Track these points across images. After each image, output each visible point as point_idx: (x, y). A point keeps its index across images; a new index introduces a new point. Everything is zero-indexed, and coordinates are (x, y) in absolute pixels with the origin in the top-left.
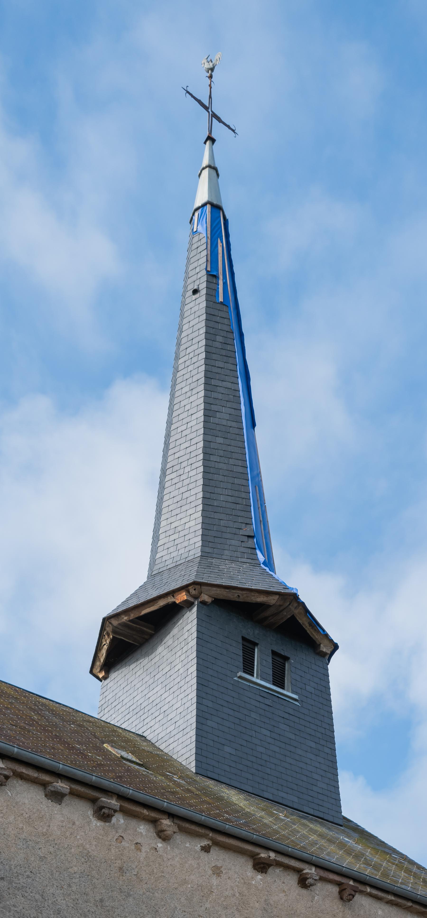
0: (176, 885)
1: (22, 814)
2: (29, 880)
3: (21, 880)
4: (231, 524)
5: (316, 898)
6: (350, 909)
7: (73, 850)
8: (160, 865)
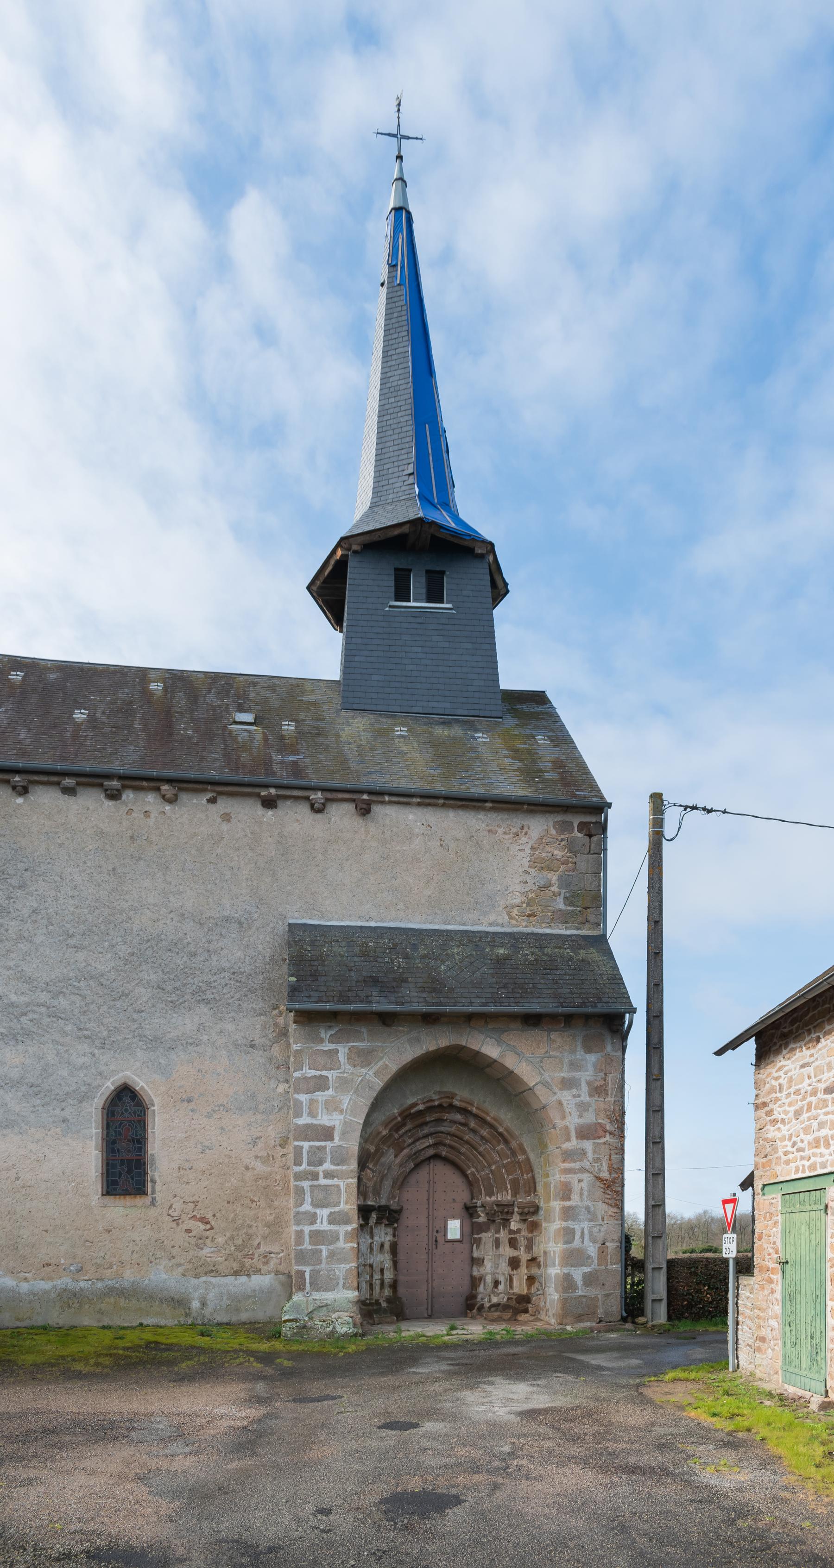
0: (186, 840)
1: (43, 813)
2: (50, 866)
3: (43, 868)
4: (396, 469)
5: (333, 819)
6: (373, 822)
7: (88, 831)
8: (169, 825)
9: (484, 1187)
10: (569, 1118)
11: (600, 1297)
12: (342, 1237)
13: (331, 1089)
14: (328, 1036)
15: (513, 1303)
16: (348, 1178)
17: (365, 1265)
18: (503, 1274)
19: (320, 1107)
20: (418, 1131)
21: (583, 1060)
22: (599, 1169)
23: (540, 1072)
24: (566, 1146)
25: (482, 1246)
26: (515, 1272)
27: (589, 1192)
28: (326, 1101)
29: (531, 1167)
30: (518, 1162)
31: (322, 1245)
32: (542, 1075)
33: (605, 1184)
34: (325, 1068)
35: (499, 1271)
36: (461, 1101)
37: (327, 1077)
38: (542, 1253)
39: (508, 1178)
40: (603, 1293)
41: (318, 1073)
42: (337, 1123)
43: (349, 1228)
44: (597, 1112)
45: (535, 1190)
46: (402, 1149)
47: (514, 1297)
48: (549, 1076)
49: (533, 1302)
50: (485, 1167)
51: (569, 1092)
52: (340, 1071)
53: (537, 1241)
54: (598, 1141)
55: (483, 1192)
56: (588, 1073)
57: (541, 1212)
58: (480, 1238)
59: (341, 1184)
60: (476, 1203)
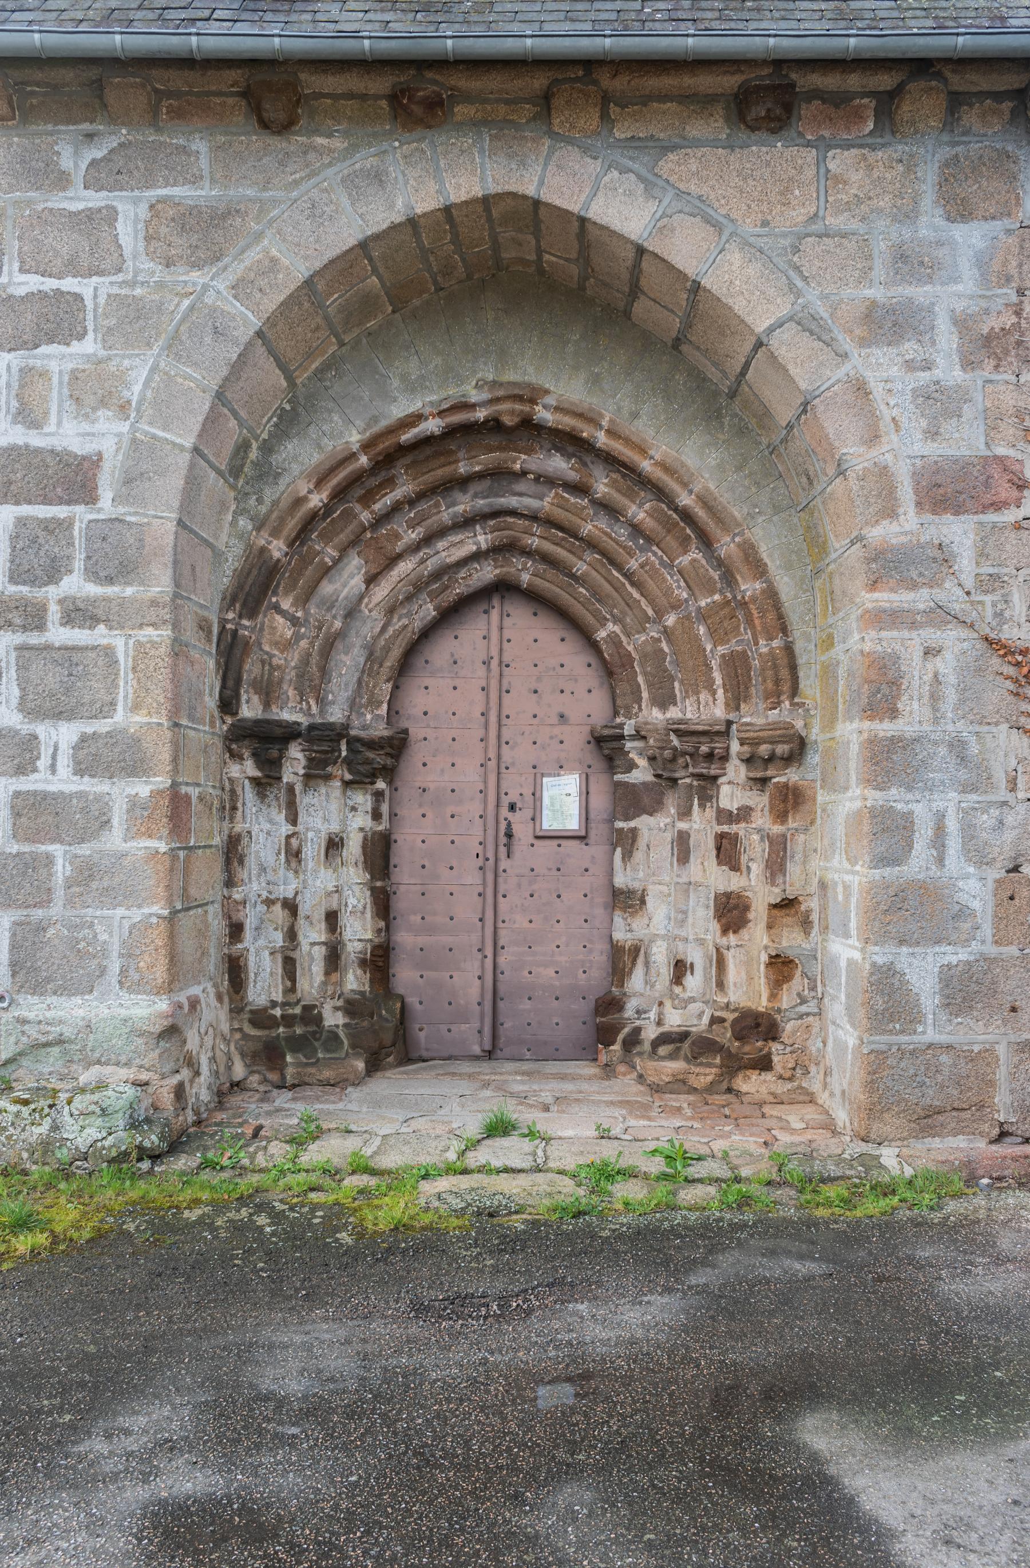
9: (647, 681)
10: (891, 440)
11: (1001, 1050)
12: (118, 817)
13: (90, 335)
14: (83, 167)
15: (725, 1036)
16: (141, 626)
17: (269, 902)
18: (701, 942)
19: (55, 394)
20: (437, 505)
21: (940, 244)
22: (999, 615)
23: (791, 286)
24: (881, 533)
25: (639, 855)
26: (732, 939)
27: (962, 690)
28: (75, 376)
29: (781, 617)
30: (744, 604)
31: (53, 841)
32: (798, 294)
33: (1018, 664)
34: (72, 268)
35: (689, 932)
36: (557, 409)
37: (78, 297)
38: (813, 887)
39: (716, 653)
40: (1012, 1038)
41: (50, 284)
42: (107, 446)
43: (142, 789)
44: (992, 420)
45: (795, 691)
46: (395, 559)
47: (730, 1017)
48: (824, 297)
49: (785, 1037)
50: (648, 619)
51: (893, 351)
52: (120, 278)
53: (799, 848)
54: (991, 517)
55: (645, 695)
56: (960, 287)
57: (813, 758)
58: (634, 831)
59: (119, 643)
60: (621, 726)
